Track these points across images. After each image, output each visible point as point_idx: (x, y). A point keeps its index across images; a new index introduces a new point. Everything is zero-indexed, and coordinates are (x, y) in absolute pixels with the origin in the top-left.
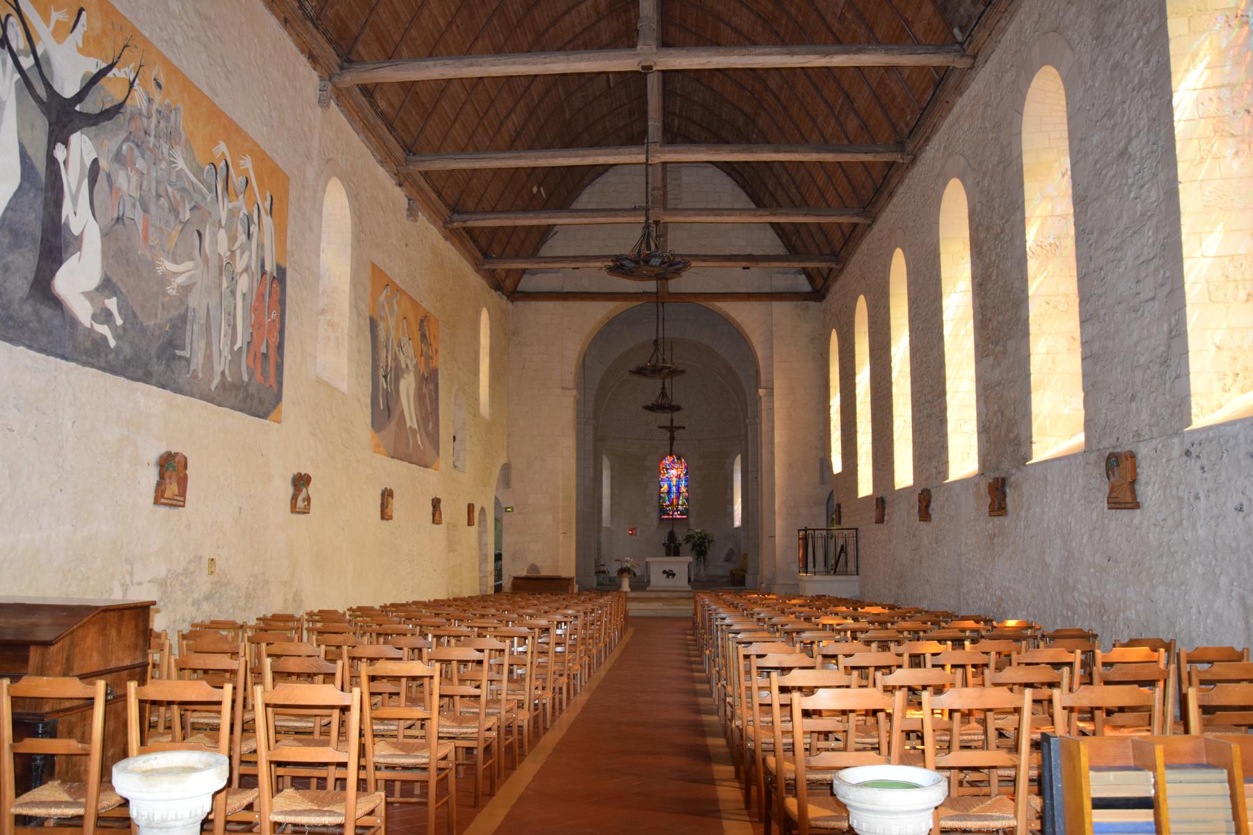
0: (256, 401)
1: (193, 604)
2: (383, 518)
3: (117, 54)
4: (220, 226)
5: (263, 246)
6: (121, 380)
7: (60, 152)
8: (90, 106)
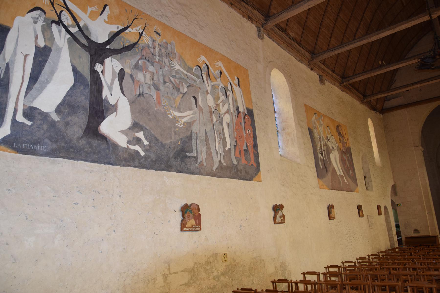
0: (244, 173)
1: (214, 279)
2: (330, 219)
3: (130, 22)
4: (207, 93)
5: (236, 101)
6: (152, 172)
7: (98, 68)
8: (114, 45)
